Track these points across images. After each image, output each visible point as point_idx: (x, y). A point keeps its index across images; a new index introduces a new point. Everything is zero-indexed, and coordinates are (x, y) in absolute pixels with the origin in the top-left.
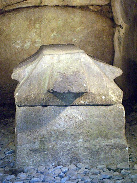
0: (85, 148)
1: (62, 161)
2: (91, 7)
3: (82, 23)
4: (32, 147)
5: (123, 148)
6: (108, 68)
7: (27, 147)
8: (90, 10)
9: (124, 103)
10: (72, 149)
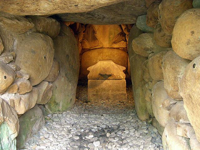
0: (112, 94)
2: (120, 48)
3: (117, 54)
5: (125, 94)
6: (121, 67)
8: (120, 49)
9: (125, 79)
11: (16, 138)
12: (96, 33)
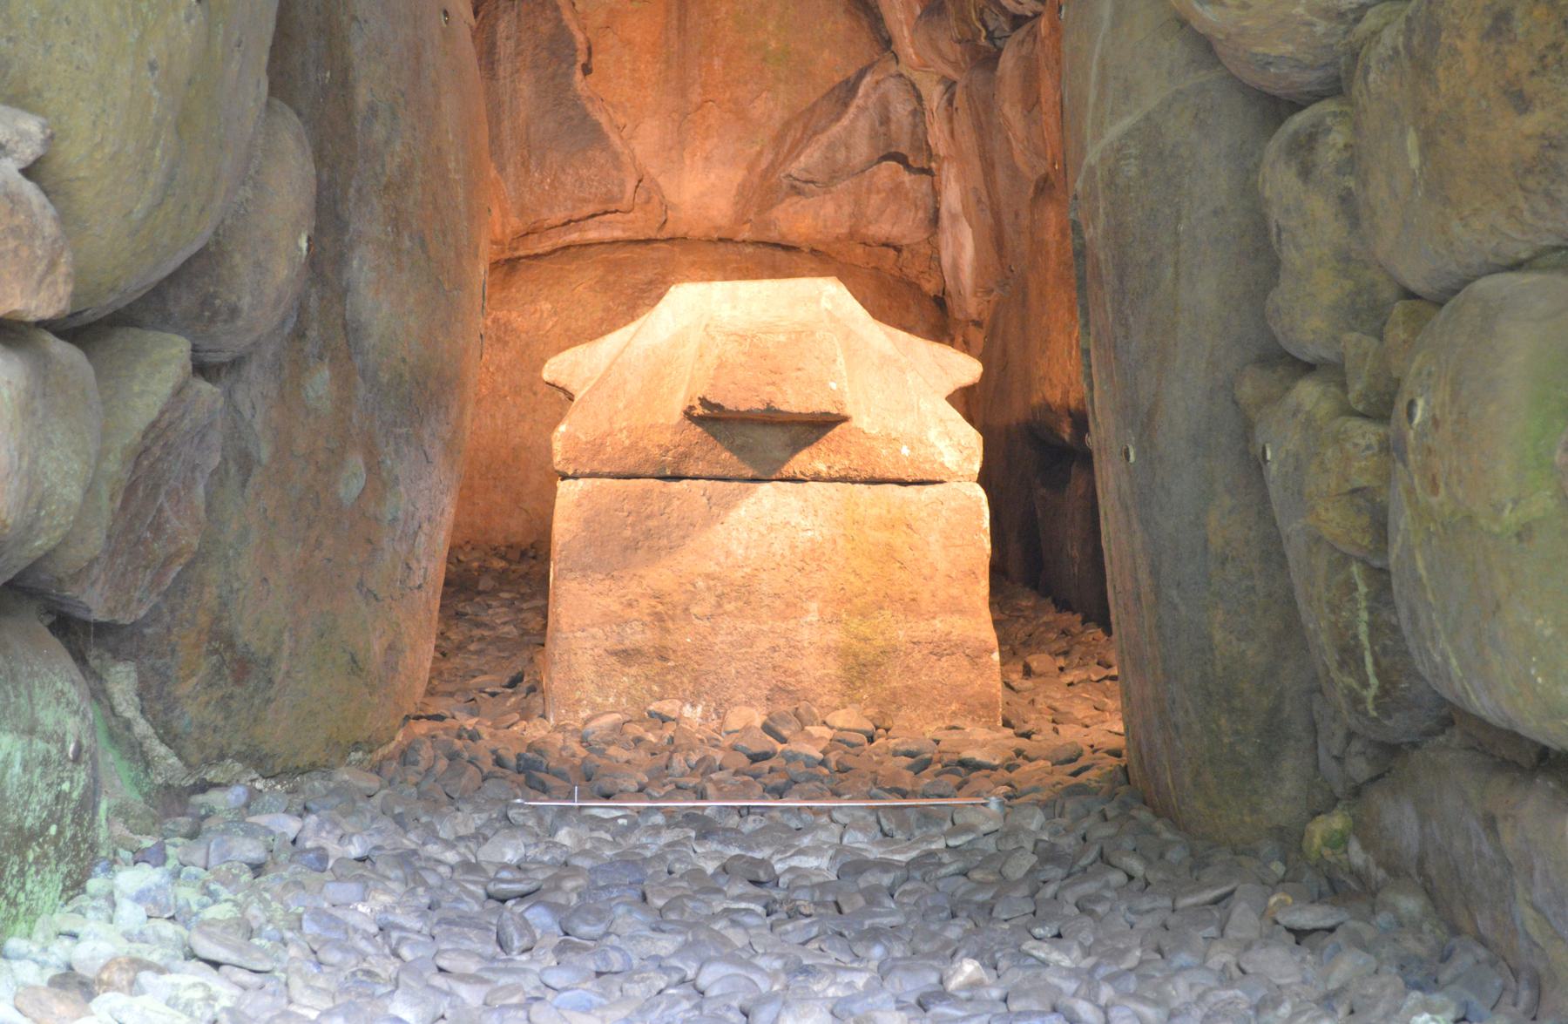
9: (984, 479)
11: (273, 91)
12: (587, 70)
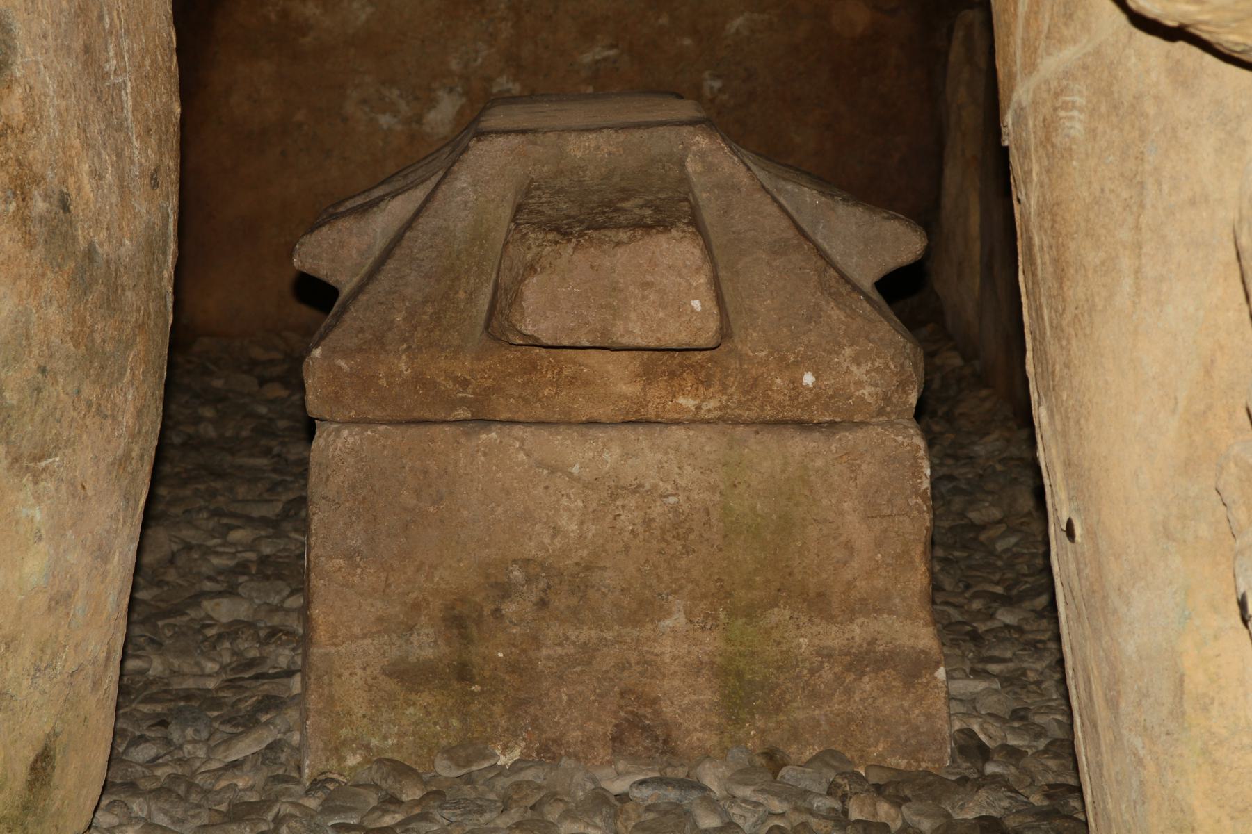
0: (697, 668)
1: (563, 735)
4: (395, 653)
7: (365, 653)
10: (624, 669)
